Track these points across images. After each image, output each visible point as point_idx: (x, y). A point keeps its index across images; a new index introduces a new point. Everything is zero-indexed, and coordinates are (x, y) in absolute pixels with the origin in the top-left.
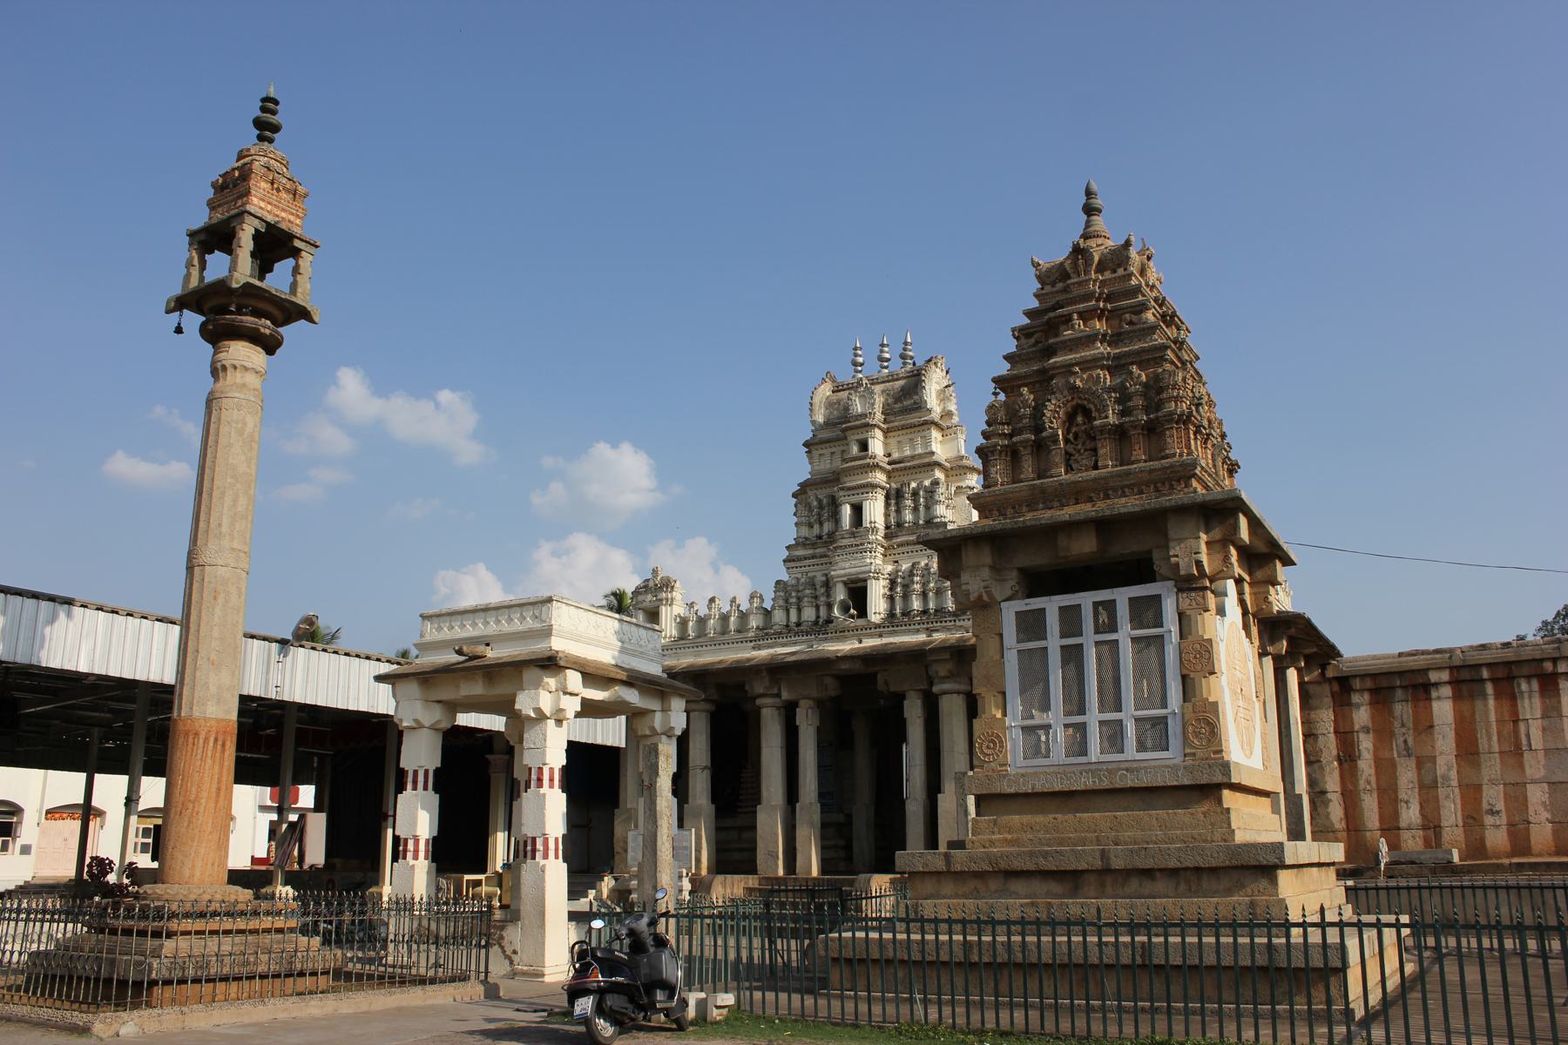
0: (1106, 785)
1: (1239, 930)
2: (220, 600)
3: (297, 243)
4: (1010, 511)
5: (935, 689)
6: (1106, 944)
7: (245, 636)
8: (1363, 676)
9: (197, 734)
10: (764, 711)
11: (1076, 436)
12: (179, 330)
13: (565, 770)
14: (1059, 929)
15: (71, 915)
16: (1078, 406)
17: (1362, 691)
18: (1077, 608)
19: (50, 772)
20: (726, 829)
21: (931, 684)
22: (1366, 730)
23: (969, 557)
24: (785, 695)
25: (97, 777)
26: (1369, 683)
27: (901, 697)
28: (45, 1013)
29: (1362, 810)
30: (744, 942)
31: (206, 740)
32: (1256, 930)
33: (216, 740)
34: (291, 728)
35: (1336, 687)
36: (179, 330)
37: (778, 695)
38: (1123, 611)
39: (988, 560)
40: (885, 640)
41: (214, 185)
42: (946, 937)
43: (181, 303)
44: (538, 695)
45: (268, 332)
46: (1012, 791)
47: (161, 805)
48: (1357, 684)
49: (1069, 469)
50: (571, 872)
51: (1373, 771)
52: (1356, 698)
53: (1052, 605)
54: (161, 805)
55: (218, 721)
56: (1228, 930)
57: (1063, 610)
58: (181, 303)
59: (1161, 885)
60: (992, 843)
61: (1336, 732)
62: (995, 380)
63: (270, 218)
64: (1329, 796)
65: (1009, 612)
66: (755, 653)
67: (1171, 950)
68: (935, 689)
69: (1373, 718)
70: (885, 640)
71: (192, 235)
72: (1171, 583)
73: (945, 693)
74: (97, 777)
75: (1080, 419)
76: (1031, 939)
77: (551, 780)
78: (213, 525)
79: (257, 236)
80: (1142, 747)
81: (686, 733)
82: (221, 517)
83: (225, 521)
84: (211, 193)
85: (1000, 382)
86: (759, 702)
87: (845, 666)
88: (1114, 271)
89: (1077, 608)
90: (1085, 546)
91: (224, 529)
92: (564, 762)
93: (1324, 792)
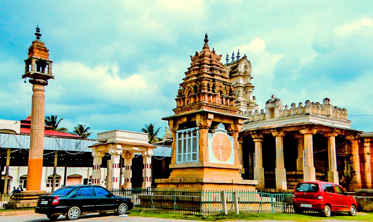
2: (37, 136)
10: (256, 144)
12: (25, 82)
20: (188, 198)
22: (368, 154)
25: (67, 168)
30: (146, 208)
34: (272, 173)
44: (117, 146)
45: (42, 82)
55: (357, 180)
61: (359, 154)
62: (180, 85)
63: (39, 58)
74: (67, 168)
79: (36, 62)
83: (37, 121)
85: (181, 85)
88: (202, 58)
91: (37, 122)
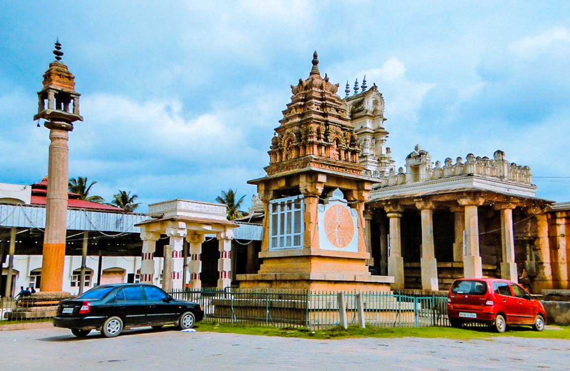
3: (72, 96)
4: (340, 112)
7: (135, 225)
8: (562, 211)
9: (49, 248)
13: (201, 255)
17: (561, 218)
19: (74, 256)
22: (563, 236)
26: (564, 215)
28: (561, 208)
29: (559, 272)
31: (52, 249)
33: (56, 249)
35: (550, 216)
47: (41, 267)
48: (559, 215)
50: (202, 282)
51: (565, 255)
52: (558, 221)
54: (41, 267)
63: (59, 89)
64: (544, 264)
69: (566, 231)
77: (226, 255)
78: (52, 186)
82: (54, 185)
83: (56, 185)
93: (542, 263)
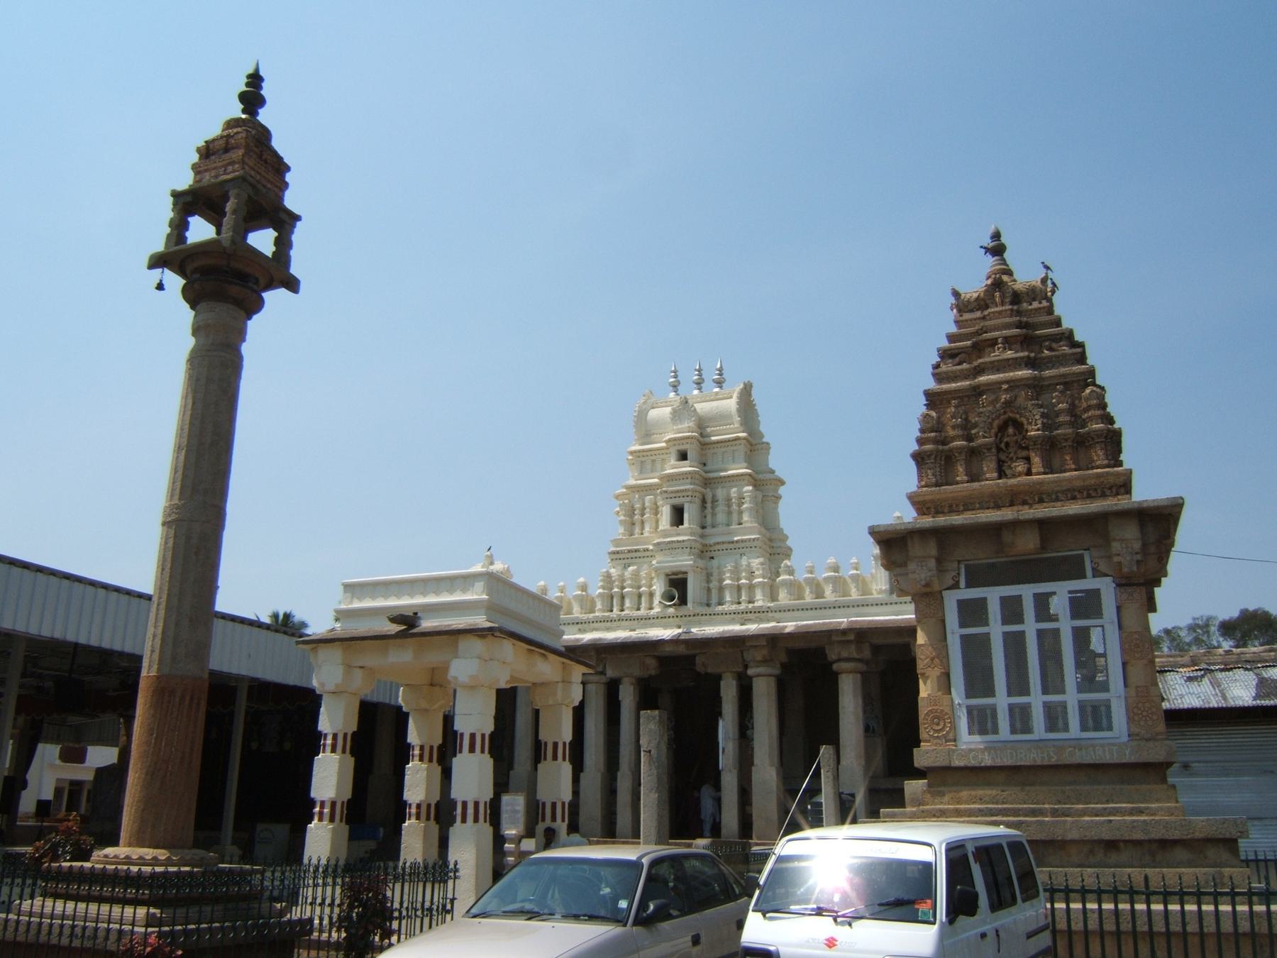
0: (1054, 761)
1: (1255, 899)
5: (750, 672)
6: (1258, 914)
11: (1007, 444)
12: (160, 287)
14: (1057, 895)
15: (677, 879)
16: (1010, 419)
18: (1018, 599)
21: (746, 667)
23: (916, 549)
24: (611, 673)
27: (718, 678)
32: (1186, 898)
36: (160, 287)
37: (603, 673)
38: (994, 609)
39: (934, 552)
40: (744, 627)
41: (199, 150)
42: (1121, 906)
43: (158, 262)
46: (962, 764)
49: (1001, 474)
53: (993, 595)
56: (1078, 896)
57: (1004, 601)
58: (158, 262)
59: (1180, 854)
60: (1055, 813)
65: (951, 600)
66: (578, 636)
67: (1222, 919)
68: (750, 672)
70: (744, 627)
71: (176, 195)
72: (1109, 579)
73: (759, 675)
75: (1011, 430)
76: (1076, 906)
80: (1084, 728)
81: (582, 703)
84: (195, 158)
86: (835, 667)
87: (668, 649)
89: (1018, 599)
90: (1027, 543)
92: (355, 729)
